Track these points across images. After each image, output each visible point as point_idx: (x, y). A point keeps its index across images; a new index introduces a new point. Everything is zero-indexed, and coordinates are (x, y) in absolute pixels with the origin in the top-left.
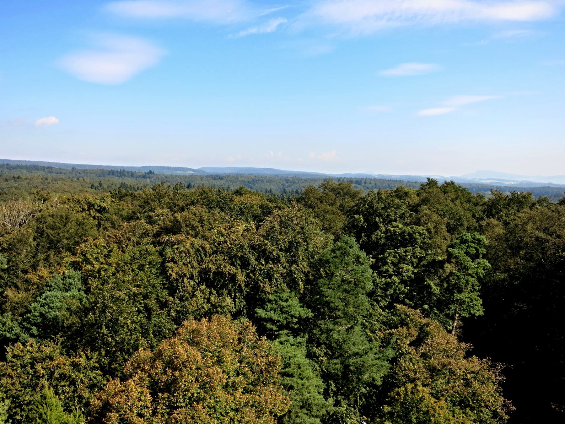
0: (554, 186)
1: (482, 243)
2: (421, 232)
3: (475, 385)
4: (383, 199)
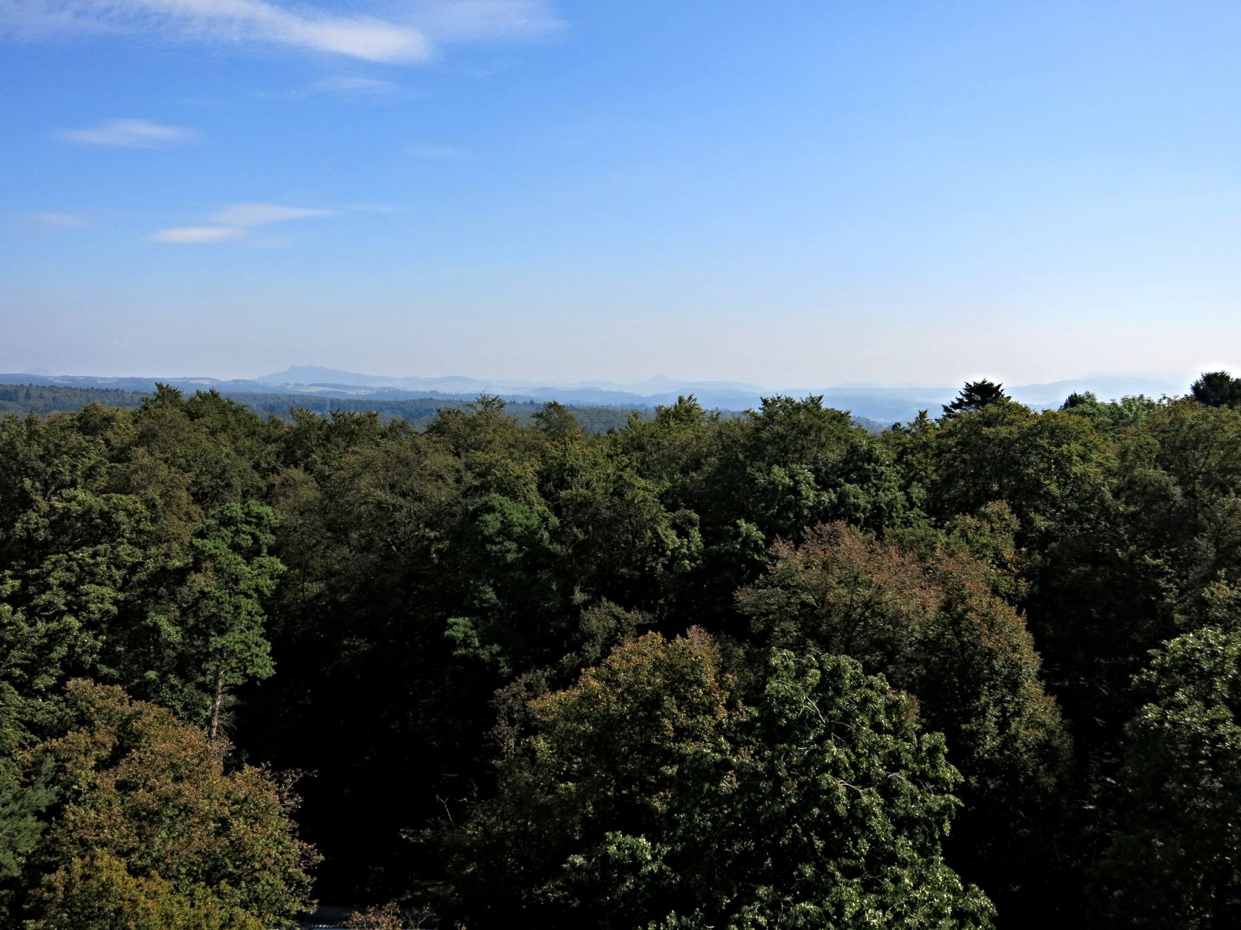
0: (440, 398)
1: (265, 522)
2: (130, 507)
3: (238, 825)
4: (40, 436)
